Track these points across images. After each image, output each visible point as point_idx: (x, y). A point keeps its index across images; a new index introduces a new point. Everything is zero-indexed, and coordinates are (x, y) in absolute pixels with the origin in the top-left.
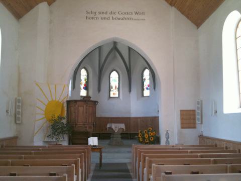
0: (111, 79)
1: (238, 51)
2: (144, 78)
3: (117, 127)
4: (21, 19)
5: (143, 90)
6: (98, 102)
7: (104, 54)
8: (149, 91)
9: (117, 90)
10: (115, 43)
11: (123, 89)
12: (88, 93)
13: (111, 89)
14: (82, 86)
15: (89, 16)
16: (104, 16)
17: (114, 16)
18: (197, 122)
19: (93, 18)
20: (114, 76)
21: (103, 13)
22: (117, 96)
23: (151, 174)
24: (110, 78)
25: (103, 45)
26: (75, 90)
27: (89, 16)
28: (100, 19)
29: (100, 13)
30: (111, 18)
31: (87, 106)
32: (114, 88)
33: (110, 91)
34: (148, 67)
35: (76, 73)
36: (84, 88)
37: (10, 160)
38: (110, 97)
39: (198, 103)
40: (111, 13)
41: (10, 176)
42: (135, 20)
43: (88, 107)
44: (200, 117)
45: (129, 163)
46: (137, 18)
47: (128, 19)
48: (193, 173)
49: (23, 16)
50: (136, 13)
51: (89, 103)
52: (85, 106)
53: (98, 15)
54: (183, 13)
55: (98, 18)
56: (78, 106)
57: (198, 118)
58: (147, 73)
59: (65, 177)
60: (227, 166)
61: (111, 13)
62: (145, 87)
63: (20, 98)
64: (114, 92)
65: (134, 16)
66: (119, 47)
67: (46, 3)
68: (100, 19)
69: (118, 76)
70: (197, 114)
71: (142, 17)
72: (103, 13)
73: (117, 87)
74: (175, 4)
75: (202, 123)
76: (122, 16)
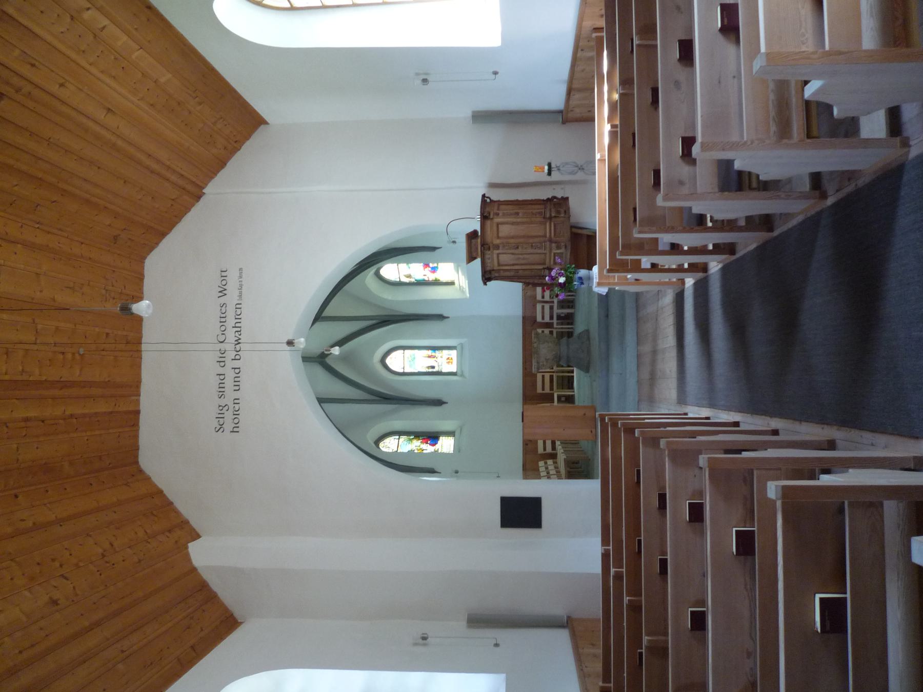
0: (407, 370)
1: (327, 3)
2: (407, 280)
4: (237, 613)
5: (437, 283)
7: (339, 389)
14: (428, 448)
15: (228, 426)
19: (236, 413)
20: (396, 361)
21: (221, 386)
23: (656, 240)
24: (404, 374)
25: (315, 395)
26: (436, 470)
27: (228, 426)
29: (221, 395)
30: (236, 364)
31: (498, 214)
32: (431, 362)
33: (439, 373)
34: (372, 270)
35: (389, 463)
36: (433, 445)
37: (626, 599)
40: (221, 362)
41: (666, 573)
42: (240, 296)
46: (237, 292)
47: (238, 317)
48: (655, 101)
49: (226, 610)
50: (223, 292)
52: (497, 220)
53: (228, 400)
54: (222, 164)
55: (236, 401)
56: (498, 237)
58: (391, 270)
60: (638, 46)
61: (221, 362)
62: (431, 277)
64: (444, 360)
65: (232, 298)
67: (190, 545)
69: (400, 352)
71: (232, 277)
72: (221, 386)
73: (430, 352)
74: (197, 185)
76: (231, 336)
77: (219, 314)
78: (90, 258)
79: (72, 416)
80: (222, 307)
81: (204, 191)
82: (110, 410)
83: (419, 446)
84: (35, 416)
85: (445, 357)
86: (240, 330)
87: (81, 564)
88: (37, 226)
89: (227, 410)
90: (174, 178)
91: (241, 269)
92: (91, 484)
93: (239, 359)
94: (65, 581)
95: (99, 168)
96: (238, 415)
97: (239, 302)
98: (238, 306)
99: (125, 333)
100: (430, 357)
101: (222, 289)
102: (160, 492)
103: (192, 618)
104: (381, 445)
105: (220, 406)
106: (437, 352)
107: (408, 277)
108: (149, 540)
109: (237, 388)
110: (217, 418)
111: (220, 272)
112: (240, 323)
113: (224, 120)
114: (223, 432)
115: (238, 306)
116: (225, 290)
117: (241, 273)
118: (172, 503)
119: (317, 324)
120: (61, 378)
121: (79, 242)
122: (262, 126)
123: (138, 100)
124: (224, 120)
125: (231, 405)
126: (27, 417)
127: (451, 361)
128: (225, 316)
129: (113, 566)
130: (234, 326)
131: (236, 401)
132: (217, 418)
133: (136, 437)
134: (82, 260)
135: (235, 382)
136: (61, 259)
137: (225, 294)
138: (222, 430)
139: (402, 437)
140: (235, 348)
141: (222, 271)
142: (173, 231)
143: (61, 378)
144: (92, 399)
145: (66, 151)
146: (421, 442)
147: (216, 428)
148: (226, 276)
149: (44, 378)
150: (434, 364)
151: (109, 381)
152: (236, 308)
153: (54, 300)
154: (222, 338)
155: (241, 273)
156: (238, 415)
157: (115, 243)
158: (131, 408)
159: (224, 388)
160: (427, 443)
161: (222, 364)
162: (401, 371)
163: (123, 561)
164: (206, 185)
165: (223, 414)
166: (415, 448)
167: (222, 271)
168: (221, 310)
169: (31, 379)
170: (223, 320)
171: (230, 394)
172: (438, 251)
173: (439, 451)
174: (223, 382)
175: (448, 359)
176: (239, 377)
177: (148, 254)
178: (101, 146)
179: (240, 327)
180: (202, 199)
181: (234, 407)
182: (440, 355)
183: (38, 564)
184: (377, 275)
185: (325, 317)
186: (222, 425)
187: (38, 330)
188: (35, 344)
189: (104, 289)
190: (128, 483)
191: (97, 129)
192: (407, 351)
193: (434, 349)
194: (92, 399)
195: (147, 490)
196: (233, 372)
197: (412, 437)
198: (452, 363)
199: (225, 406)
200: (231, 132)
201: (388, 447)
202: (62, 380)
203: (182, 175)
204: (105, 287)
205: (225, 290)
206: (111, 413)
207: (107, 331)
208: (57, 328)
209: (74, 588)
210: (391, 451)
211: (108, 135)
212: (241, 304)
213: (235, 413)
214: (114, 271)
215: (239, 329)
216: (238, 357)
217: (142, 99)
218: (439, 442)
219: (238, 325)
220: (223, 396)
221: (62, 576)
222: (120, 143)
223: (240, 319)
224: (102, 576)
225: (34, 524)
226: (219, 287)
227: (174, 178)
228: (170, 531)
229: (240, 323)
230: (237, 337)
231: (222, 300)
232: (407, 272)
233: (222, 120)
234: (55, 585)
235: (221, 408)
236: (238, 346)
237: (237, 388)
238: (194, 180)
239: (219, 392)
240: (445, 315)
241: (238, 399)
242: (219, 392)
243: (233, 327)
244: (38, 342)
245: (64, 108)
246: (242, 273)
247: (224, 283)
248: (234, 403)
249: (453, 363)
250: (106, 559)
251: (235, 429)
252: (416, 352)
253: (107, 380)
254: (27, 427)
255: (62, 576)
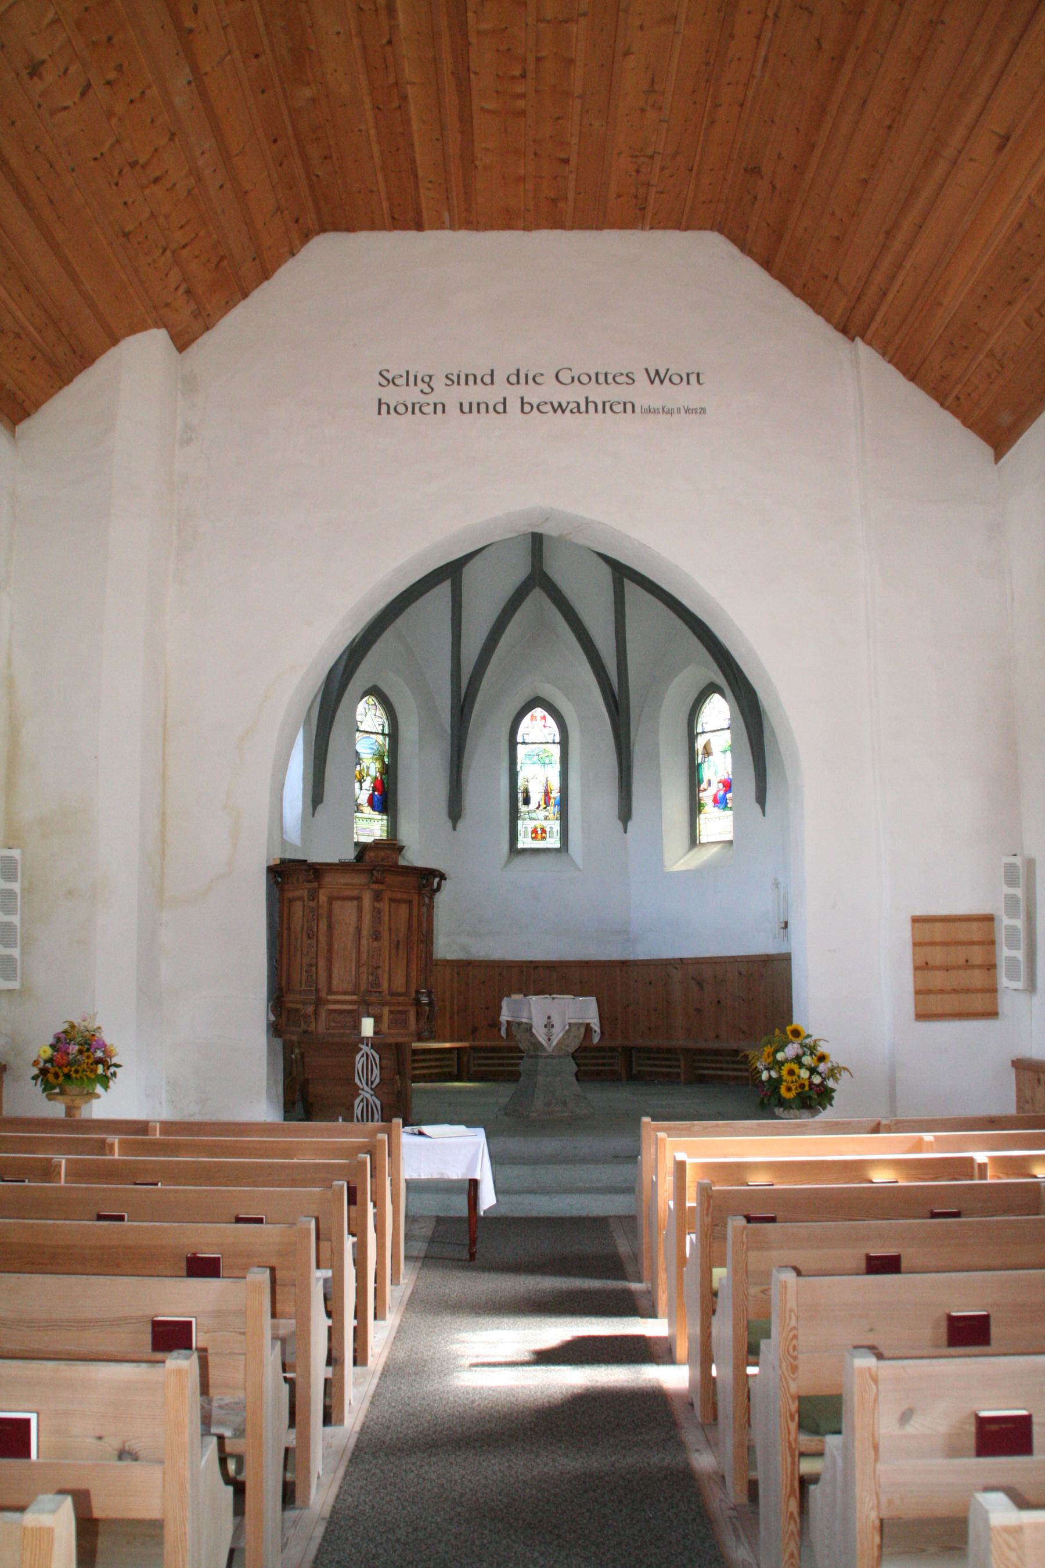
0: (521, 750)
2: (700, 744)
3: (565, 1037)
5: (695, 807)
6: (442, 877)
8: (729, 813)
9: (553, 810)
10: (537, 540)
11: (405, 1265)
12: (393, 827)
13: (523, 808)
15: (392, 395)
16: (474, 393)
17: (533, 394)
18: (1004, 982)
19: (414, 408)
22: (553, 842)
24: (513, 745)
26: (320, 808)
27: (392, 395)
28: (453, 409)
30: (514, 406)
31: (377, 897)
32: (536, 797)
33: (514, 815)
34: (721, 680)
36: (371, 802)
38: (514, 850)
39: (1011, 876)
40: (517, 377)
43: (385, 905)
44: (1020, 954)
45: (620, 1218)
46: (657, 404)
47: (607, 407)
49: (37, 405)
50: (656, 377)
51: (390, 879)
53: (442, 392)
54: (912, 374)
56: (331, 900)
57: (1012, 961)
59: (365, 1163)
61: (517, 377)
62: (706, 796)
63: (16, 853)
65: (643, 393)
66: (559, 571)
68: (453, 409)
70: (1001, 936)
73: (555, 794)
75: (1031, 987)
76: (573, 394)
77: (612, 371)
78: (713, 122)
79: (404, 98)
80: (627, 376)
81: (858, 340)
82: (420, 173)
83: (368, 775)
84: (398, 25)
85: (547, 825)
86: (581, 410)
87: (114, 121)
88: (770, 14)
89: (422, 391)
90: (879, 278)
91: (703, 411)
92: (275, 141)
93: (522, 411)
94: (80, 90)
95: (890, 127)
96: (413, 412)
97: (638, 409)
98: (629, 407)
99: (571, 195)
100: (547, 794)
101: (662, 376)
102: (266, 274)
103: (18, 336)
104: (371, 700)
105: (430, 377)
106: (557, 809)
107: (705, 747)
108: (168, 253)
109: (466, 409)
110: (408, 373)
111: (696, 371)
112: (596, 411)
113: (998, 372)
114: (380, 384)
115: (629, 407)
116: (662, 382)
117: (694, 411)
118: (245, 295)
119: (606, 570)
120: (476, 73)
121: (744, 100)
122: (988, 451)
123: (1029, 197)
124: (998, 372)
125: (431, 399)
126: (395, 11)
127: (539, 837)
128: (609, 382)
129: (112, 184)
130: (589, 400)
131: (439, 408)
132: (408, 373)
133: (373, 226)
134: (709, 104)
135: (479, 404)
136: (707, 64)
137: (652, 382)
138: (385, 383)
139: (387, 739)
140: (546, 403)
141: (698, 375)
142: (776, 283)
143: (476, 73)
144: (438, 136)
145: (920, 59)
146: (376, 778)
147: (388, 371)
148: (688, 383)
149: (473, 40)
150: (533, 805)
151: (476, 167)
152: (625, 404)
153: (627, 53)
154: (565, 377)
155: (694, 411)
156: (413, 412)
157: (746, 170)
158: (425, 216)
159: (467, 383)
160: (374, 789)
161: (513, 379)
162: (519, 739)
163: (125, 203)
164: (870, 344)
165: (415, 384)
166: (364, 765)
167: (698, 375)
168: (622, 374)
169: (470, 14)
170: (601, 379)
171: (452, 396)
172: (757, 808)
173: (358, 815)
174: (479, 381)
175: (543, 831)
176: (487, 411)
177: (728, 237)
178: (933, 129)
179: (587, 411)
180: (840, 335)
181: (428, 404)
182: (551, 816)
183: (110, 39)
184: (711, 689)
185: (623, 586)
186: (394, 383)
187: (566, 25)
188: (539, 20)
189: (655, 152)
190: (282, 212)
191: (968, 117)
192: (556, 751)
193: (563, 804)
194: (438, 136)
195: (270, 248)
196: (498, 401)
197: (386, 760)
198: (534, 838)
199: (429, 385)
200: (977, 388)
201: (366, 714)
202: (472, 76)
203: (885, 294)
204: (659, 153)
205: (662, 382)
206: (416, 176)
207: (573, 162)
208: (571, 62)
209: (66, 108)
210: (358, 718)
211: (956, 141)
212: (633, 411)
213: (417, 407)
214: (691, 170)
215: (583, 408)
216: (527, 408)
217: (1030, 202)
218: (376, 815)
219: (591, 406)
220: (449, 382)
221: (89, 85)
222: (941, 168)
223: (604, 411)
224: (93, 163)
225: (190, 31)
226: (668, 370)
227: (879, 278)
228: (188, 292)
229: (596, 411)
230: (567, 407)
231: (641, 378)
232: (715, 748)
233: (999, 369)
234: (69, 72)
235: (427, 379)
236: (549, 408)
237: (466, 409)
238: (878, 319)
239: (459, 376)
240: (631, 825)
241: (444, 412)
242: (459, 376)
243: (587, 398)
244: (542, 25)
245: (1004, 48)
246: (696, 413)
247: (675, 379)
248: (435, 405)
249: (534, 842)
250: (127, 169)
251: (384, 408)
252: (557, 768)
253: (477, 163)
254: (376, 11)
255: (89, 85)
